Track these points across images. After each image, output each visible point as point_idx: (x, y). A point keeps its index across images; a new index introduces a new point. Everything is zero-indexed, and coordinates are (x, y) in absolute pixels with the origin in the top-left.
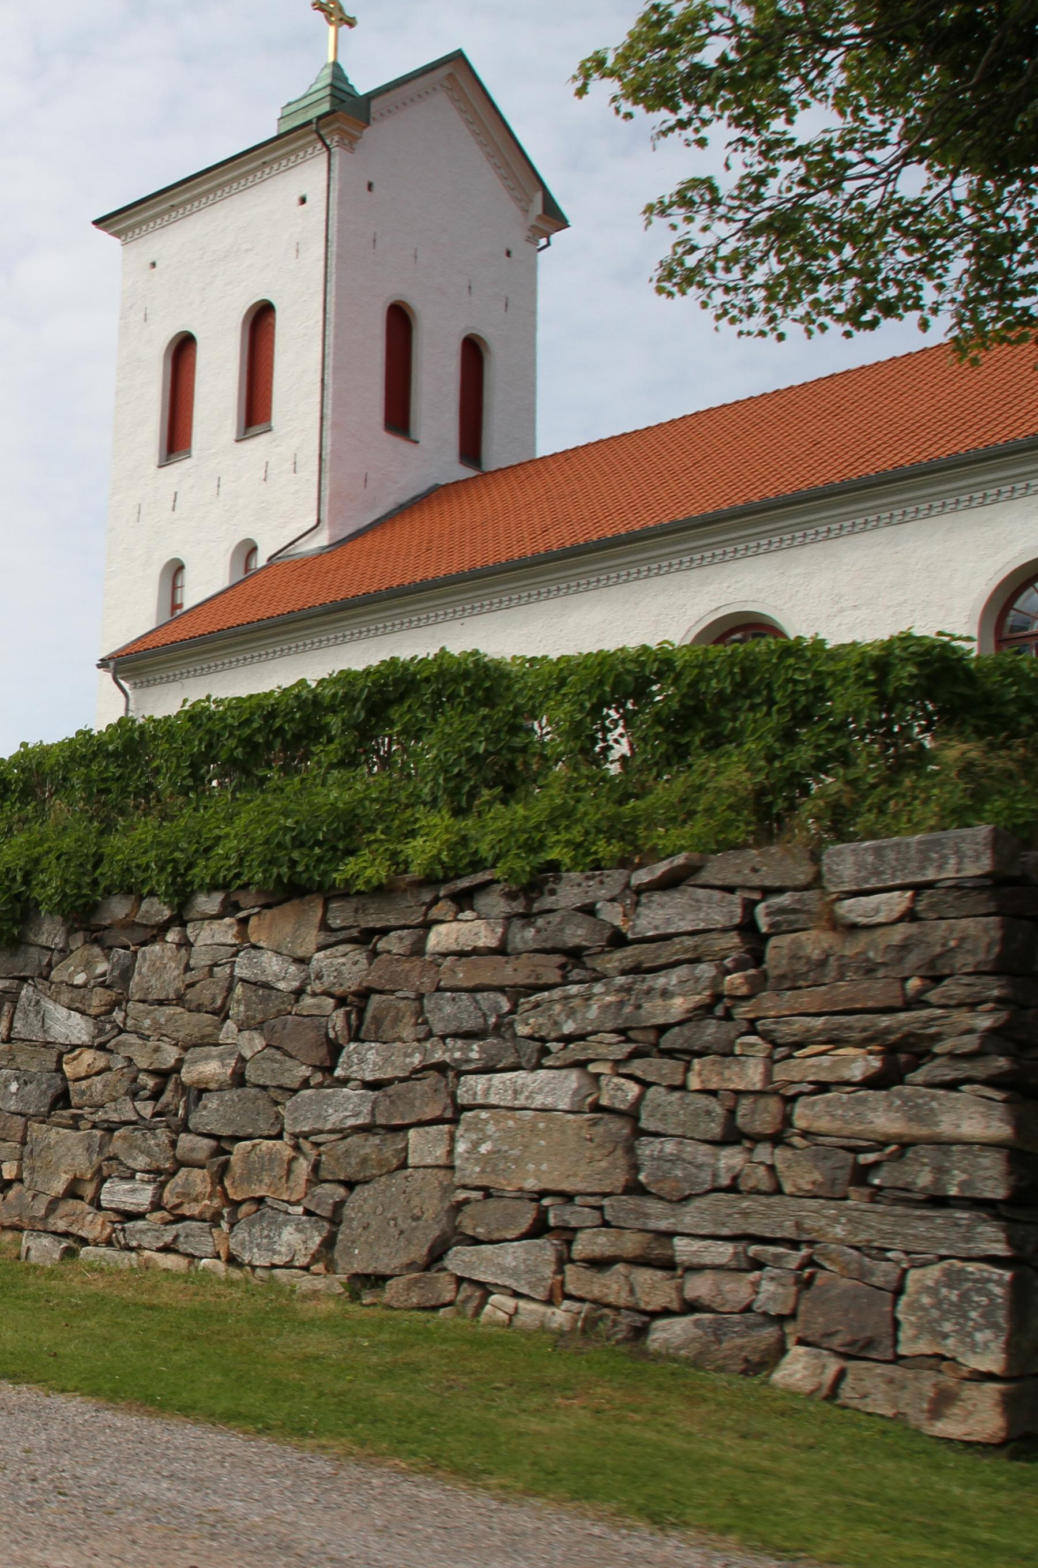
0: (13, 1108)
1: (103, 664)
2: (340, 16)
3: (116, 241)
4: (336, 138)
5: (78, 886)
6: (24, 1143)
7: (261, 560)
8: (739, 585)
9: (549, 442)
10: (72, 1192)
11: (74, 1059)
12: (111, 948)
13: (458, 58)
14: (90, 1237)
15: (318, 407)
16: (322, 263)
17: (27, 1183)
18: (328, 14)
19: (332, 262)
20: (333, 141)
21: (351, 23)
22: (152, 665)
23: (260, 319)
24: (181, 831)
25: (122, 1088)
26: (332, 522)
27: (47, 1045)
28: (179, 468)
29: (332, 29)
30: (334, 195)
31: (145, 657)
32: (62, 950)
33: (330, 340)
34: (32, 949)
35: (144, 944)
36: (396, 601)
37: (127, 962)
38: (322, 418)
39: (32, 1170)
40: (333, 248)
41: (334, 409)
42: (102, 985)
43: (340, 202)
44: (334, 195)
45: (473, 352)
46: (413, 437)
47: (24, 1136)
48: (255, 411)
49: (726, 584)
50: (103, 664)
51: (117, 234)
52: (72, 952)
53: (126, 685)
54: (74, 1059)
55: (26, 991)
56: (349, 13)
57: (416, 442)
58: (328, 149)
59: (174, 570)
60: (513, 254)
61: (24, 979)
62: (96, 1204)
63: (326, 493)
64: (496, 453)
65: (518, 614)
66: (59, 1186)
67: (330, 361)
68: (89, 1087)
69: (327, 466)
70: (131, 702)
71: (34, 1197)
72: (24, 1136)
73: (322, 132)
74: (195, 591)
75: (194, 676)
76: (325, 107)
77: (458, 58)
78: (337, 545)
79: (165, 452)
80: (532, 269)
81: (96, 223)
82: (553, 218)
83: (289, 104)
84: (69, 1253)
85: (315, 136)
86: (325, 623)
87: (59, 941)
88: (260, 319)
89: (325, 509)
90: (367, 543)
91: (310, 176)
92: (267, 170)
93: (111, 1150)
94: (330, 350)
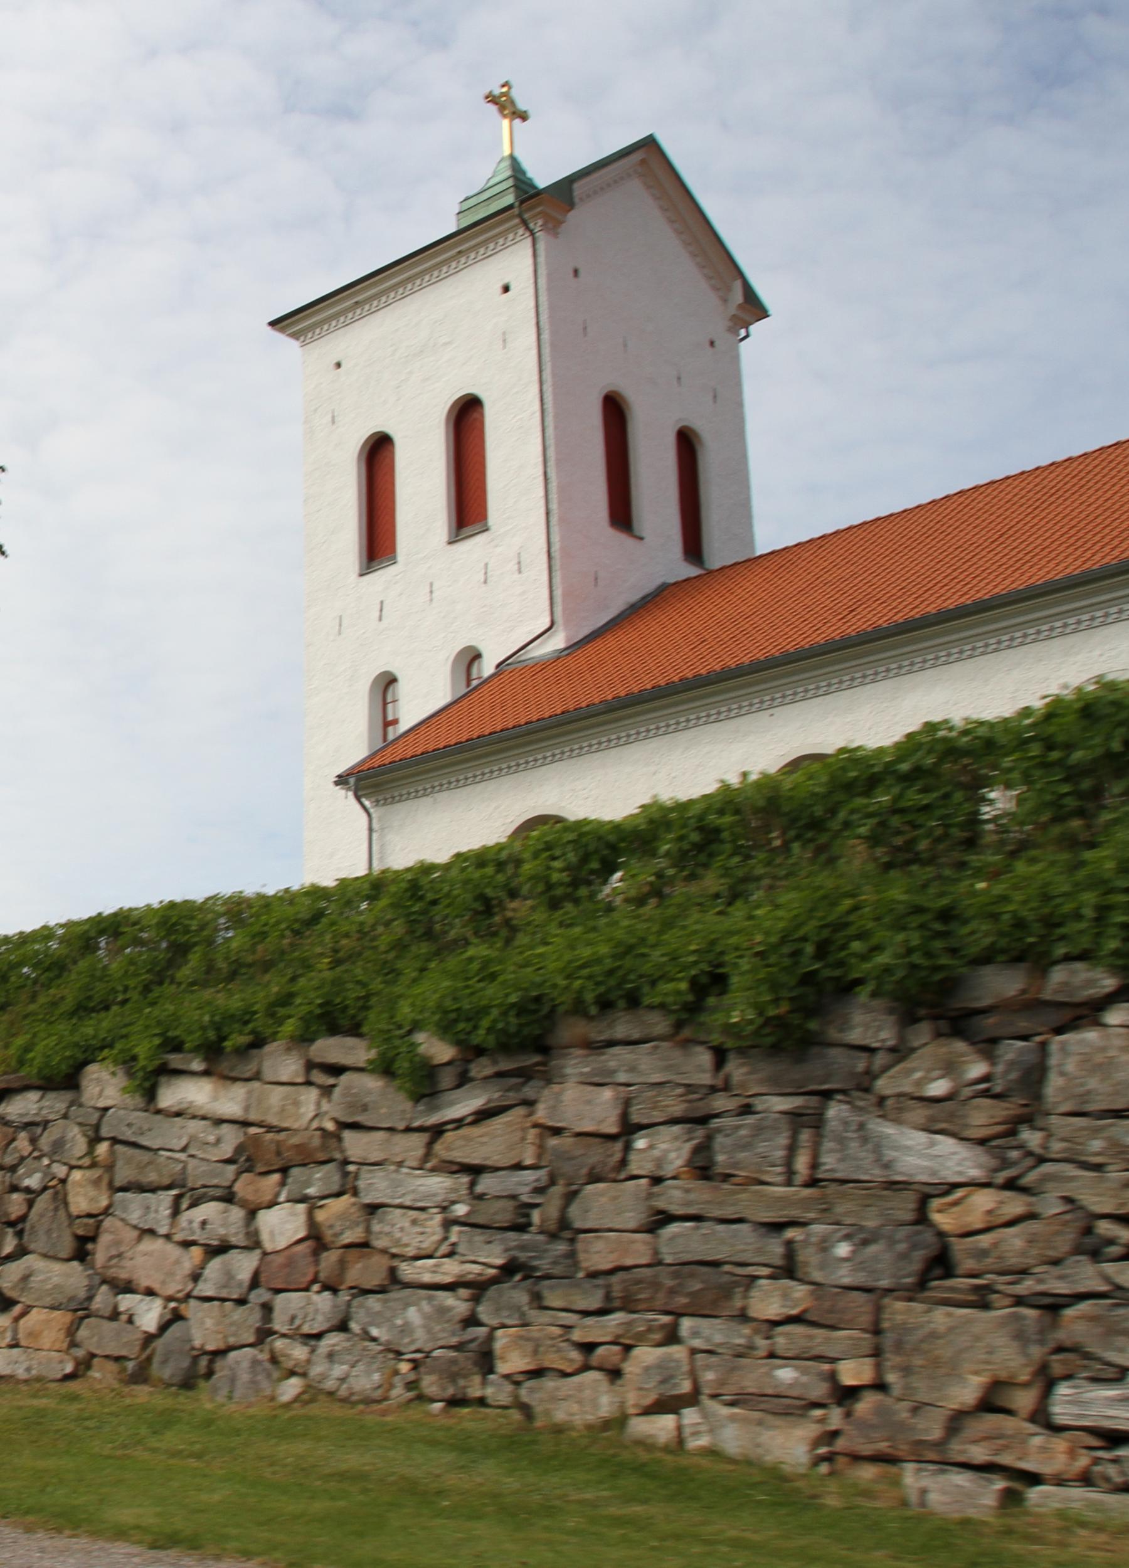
0: (846, 1281)
1: (341, 780)
2: (513, 110)
3: (294, 344)
4: (540, 222)
5: (929, 955)
6: (877, 1331)
7: (487, 667)
8: (1114, 653)
9: (769, 536)
10: (989, 1404)
11: (956, 1203)
12: (994, 1041)
13: (649, 144)
14: (1045, 1469)
15: (542, 502)
16: (534, 352)
17: (896, 1391)
18: (502, 108)
19: (546, 351)
20: (537, 225)
21: (523, 116)
22: (393, 781)
23: (466, 415)
24: (269, 982)
25: (1063, 1243)
26: (567, 622)
27: (891, 1185)
28: (382, 577)
29: (506, 123)
30: (542, 282)
31: (391, 771)
32: (892, 1050)
33: (550, 431)
34: (833, 1052)
35: (1059, 1031)
36: (690, 694)
37: (1032, 1058)
38: (548, 513)
39: (906, 1371)
40: (546, 336)
41: (560, 503)
42: (986, 1094)
43: (549, 289)
44: (542, 282)
45: (687, 444)
46: (637, 532)
47: (877, 1322)
48: (467, 510)
49: (1097, 652)
50: (341, 780)
51: (295, 336)
52: (913, 1050)
53: (367, 803)
54: (956, 1203)
55: (835, 1111)
56: (521, 106)
57: (641, 539)
58: (532, 234)
59: (383, 685)
60: (717, 343)
61: (827, 1095)
62: (1041, 1418)
63: (558, 593)
64: (718, 553)
65: (842, 699)
66: (967, 1392)
67: (551, 453)
68: (995, 1245)
69: (557, 564)
70: (375, 821)
71: (915, 1410)
72: (877, 1322)
73: (526, 216)
74: (414, 707)
75: (448, 789)
76: (509, 199)
77: (649, 144)
78: (574, 647)
79: (454, 525)
80: (735, 359)
81: (273, 324)
82: (753, 308)
83: (466, 199)
84: (1010, 1498)
85: (517, 221)
86: (593, 726)
87: (886, 1035)
88: (466, 415)
89: (558, 609)
90: (611, 641)
91: (515, 262)
92: (463, 260)
93: (1061, 1336)
94: (551, 442)
